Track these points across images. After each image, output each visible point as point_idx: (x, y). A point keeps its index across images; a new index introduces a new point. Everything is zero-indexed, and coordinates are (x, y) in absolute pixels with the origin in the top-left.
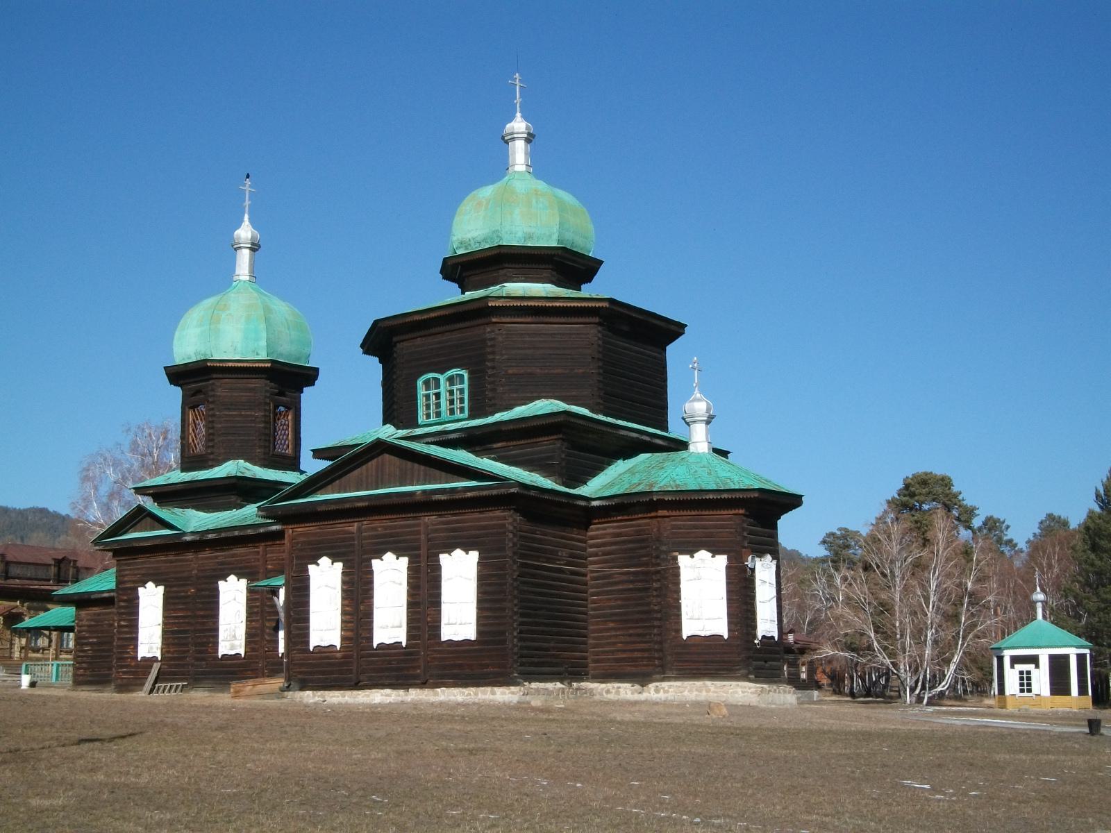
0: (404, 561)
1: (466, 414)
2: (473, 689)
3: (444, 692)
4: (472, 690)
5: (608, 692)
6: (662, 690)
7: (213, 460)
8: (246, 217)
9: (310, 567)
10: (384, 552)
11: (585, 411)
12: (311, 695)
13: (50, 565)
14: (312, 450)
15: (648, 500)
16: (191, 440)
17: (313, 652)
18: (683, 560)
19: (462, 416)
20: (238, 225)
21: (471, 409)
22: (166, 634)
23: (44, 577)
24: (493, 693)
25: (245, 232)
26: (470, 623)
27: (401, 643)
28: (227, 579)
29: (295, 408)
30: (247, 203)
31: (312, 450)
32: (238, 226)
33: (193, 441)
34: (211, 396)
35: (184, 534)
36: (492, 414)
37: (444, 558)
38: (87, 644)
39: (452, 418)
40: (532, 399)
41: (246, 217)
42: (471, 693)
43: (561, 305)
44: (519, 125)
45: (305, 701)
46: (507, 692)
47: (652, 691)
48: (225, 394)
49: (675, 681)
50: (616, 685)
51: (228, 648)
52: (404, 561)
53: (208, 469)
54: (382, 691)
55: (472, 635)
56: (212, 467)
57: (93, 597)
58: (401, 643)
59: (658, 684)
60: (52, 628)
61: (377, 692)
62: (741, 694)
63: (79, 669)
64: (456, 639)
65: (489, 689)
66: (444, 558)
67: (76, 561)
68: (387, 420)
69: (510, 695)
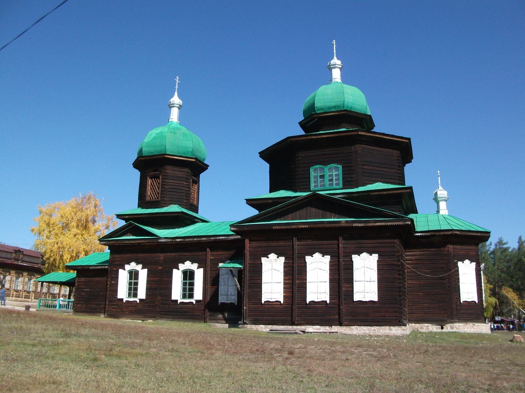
0: (328, 258)
1: (341, 186)
2: (377, 327)
3: (357, 329)
4: (376, 328)
5: (421, 328)
6: (455, 328)
7: (163, 203)
8: (176, 93)
9: (262, 258)
10: (362, 252)
11: (308, 199)
12: (264, 327)
13: (13, 253)
14: (116, 215)
15: (450, 233)
16: (149, 193)
17: (264, 304)
18: (460, 264)
19: (338, 187)
20: (172, 96)
21: (344, 182)
22: (148, 289)
23: (10, 258)
24: (390, 330)
25: (176, 100)
26: (474, 293)
27: (326, 301)
28: (185, 263)
29: (196, 182)
30: (177, 87)
31: (116, 215)
32: (172, 97)
33: (151, 194)
34: (164, 172)
35: (160, 238)
36: (357, 187)
37: (308, 259)
38: (83, 292)
39: (331, 187)
40: (375, 182)
41: (176, 93)
42: (376, 329)
43: (390, 138)
44: (336, 61)
45: (260, 330)
46: (400, 329)
47: (449, 328)
48: (170, 172)
49: (458, 323)
50: (426, 325)
51: (226, 299)
52: (328, 258)
53: (167, 206)
54: (314, 327)
55: (376, 299)
56: (163, 207)
57: (91, 268)
58: (326, 301)
59: (451, 325)
60: (58, 282)
61: (310, 327)
62: (485, 330)
63: (77, 304)
64: (364, 300)
65: (387, 327)
66: (308, 259)
67: (23, 252)
68: (139, 206)
69: (402, 331)
